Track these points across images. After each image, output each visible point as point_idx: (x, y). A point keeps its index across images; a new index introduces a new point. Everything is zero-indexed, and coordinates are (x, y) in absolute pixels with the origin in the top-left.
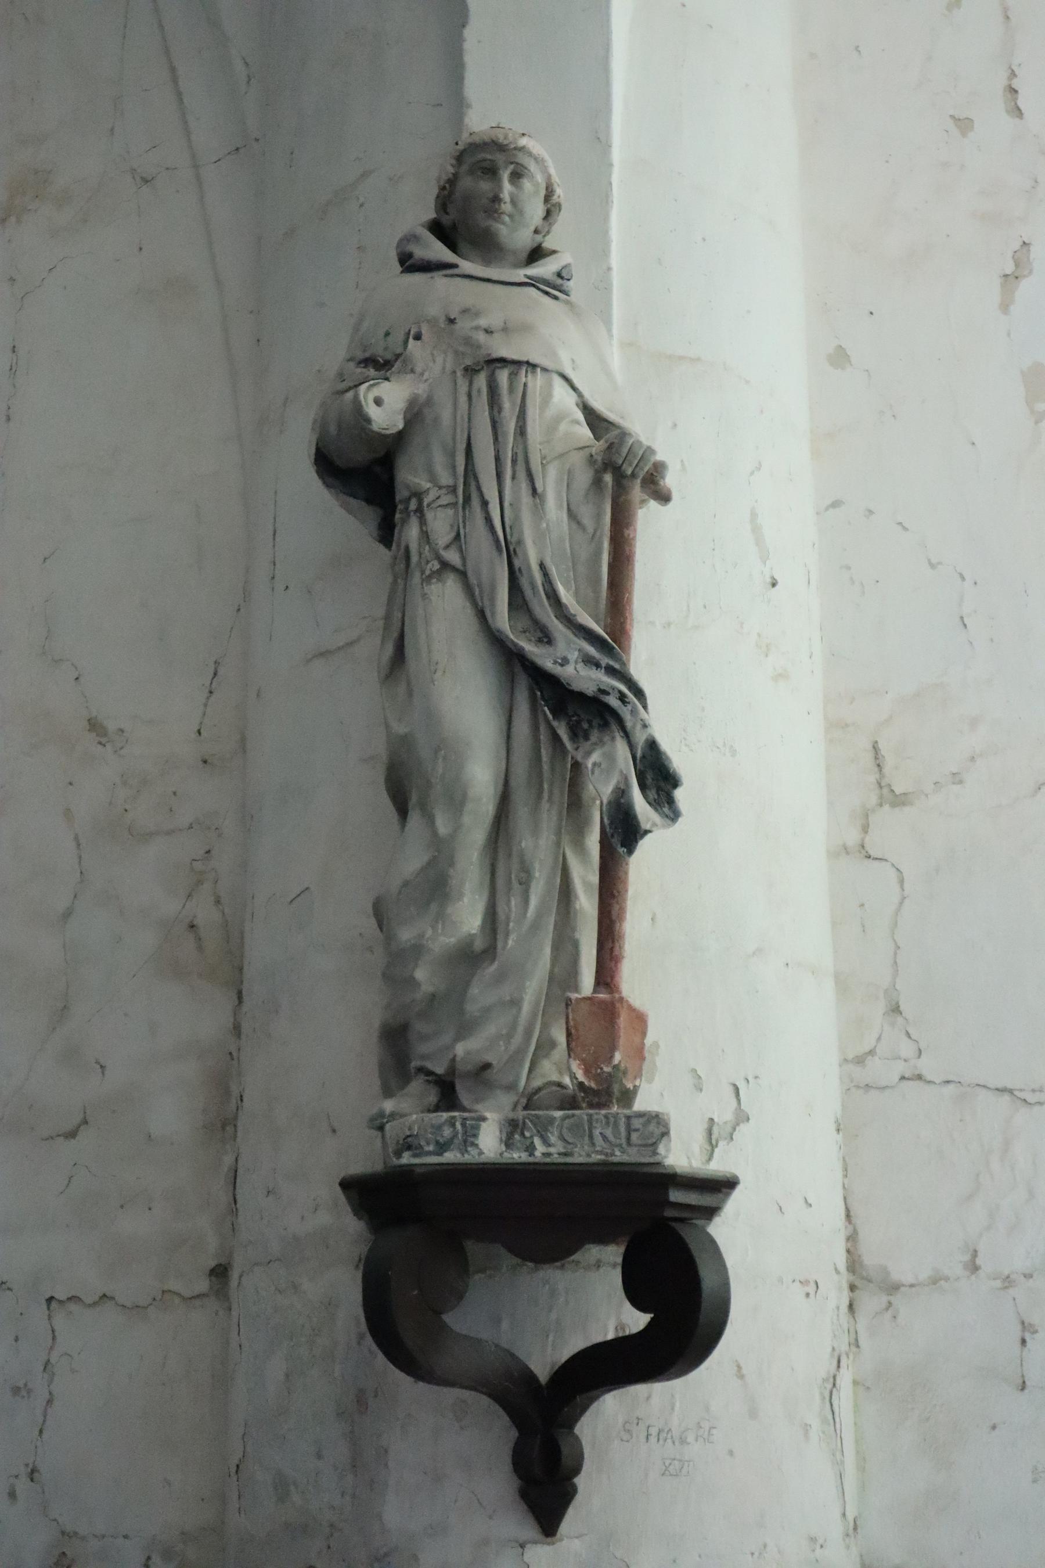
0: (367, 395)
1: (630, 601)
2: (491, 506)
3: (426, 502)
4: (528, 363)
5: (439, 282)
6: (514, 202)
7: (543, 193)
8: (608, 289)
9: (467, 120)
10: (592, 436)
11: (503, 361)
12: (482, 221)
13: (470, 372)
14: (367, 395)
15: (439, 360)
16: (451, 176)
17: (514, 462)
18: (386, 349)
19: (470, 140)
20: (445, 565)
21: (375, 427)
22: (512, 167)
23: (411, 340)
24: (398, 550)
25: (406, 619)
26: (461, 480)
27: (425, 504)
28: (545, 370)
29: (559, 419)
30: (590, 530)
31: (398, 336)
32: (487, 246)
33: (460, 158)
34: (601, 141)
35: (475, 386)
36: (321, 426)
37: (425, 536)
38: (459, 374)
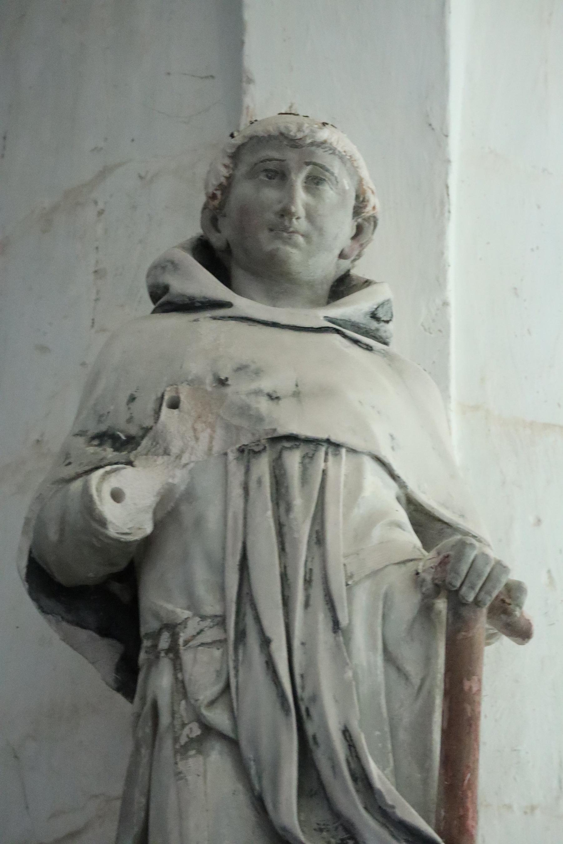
0: (100, 485)
1: (472, 785)
2: (274, 646)
3: (183, 637)
4: (328, 441)
5: (205, 325)
6: (310, 217)
7: (352, 202)
8: (443, 332)
9: (247, 101)
10: (418, 543)
11: (293, 438)
12: (267, 242)
13: (248, 453)
14: (100, 485)
15: (204, 436)
16: (223, 180)
17: (308, 582)
18: (130, 420)
19: (249, 132)
20: (208, 730)
21: (112, 532)
22: (309, 168)
23: (164, 409)
24: (143, 704)
25: (152, 805)
26: (233, 608)
27: (181, 641)
28: (352, 451)
29: (371, 521)
30: (416, 680)
31: (147, 403)
32: (273, 276)
33: (236, 156)
34: (434, 130)
35: (254, 477)
36: (37, 527)
37: (181, 688)
38: (231, 456)
